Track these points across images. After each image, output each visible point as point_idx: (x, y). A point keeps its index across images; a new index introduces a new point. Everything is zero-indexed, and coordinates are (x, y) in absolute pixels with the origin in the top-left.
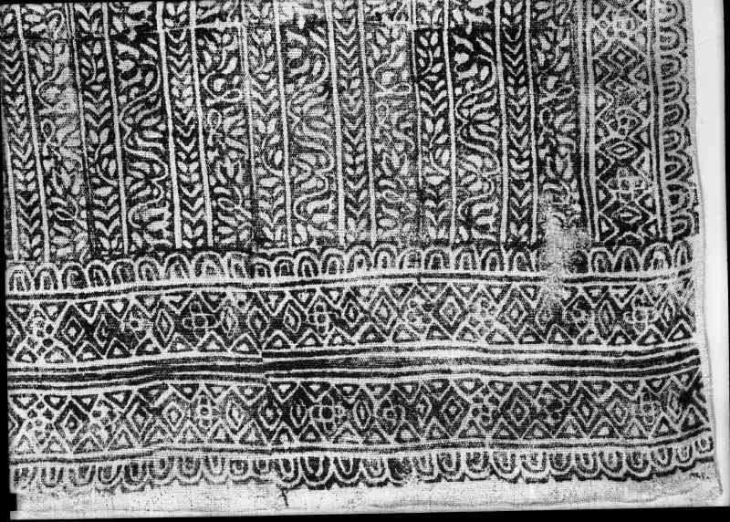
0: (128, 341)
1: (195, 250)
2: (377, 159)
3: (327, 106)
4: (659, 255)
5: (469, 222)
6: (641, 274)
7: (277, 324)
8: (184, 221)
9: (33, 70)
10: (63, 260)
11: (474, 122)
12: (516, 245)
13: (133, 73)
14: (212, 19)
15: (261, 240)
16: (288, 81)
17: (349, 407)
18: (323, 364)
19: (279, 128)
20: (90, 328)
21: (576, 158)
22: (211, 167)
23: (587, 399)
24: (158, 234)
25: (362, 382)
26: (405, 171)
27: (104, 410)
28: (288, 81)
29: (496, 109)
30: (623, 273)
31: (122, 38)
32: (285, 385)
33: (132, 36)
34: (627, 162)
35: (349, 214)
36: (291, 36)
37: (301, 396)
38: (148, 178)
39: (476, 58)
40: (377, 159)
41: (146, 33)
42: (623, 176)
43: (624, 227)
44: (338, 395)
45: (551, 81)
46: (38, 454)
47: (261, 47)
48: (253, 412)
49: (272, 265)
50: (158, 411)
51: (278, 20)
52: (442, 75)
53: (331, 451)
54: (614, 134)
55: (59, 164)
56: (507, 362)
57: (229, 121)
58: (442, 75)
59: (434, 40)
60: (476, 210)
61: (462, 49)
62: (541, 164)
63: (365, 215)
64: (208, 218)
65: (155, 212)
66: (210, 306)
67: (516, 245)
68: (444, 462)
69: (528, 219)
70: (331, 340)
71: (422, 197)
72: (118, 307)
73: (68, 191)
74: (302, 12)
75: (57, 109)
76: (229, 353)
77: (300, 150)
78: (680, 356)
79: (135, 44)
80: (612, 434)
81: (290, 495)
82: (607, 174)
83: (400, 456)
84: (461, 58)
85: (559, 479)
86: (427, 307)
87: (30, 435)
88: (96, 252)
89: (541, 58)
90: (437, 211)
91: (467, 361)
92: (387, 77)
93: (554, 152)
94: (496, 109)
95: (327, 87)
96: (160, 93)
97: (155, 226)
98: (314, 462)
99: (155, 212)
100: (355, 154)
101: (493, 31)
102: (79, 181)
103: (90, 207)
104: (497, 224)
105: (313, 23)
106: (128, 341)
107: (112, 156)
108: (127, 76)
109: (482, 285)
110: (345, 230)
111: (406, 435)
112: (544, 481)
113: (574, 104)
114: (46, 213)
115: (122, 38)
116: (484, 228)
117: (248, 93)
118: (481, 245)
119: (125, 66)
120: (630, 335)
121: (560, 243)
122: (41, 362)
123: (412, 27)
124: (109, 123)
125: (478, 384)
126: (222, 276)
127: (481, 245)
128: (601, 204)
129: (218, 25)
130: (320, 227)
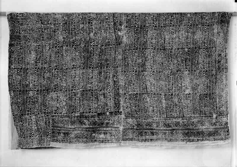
0: (170, 126)
1: (177, 117)
2: (196, 108)
3: (191, 103)
4: (225, 117)
5: (205, 114)
6: (223, 119)
7: (186, 125)
8: (176, 114)
9: (160, 98)
10: (163, 118)
11: (206, 104)
12: (210, 116)
13: (170, 99)
14: (179, 93)
15: (184, 116)
16: (187, 100)
17: (193, 134)
18: (190, 129)
19: (186, 105)
20: (166, 125)
21: (216, 107)
22: (179, 109)
23: (217, 132)
24: (173, 116)
25: (194, 131)
26: (199, 109)
27: (168, 134)
28: (187, 100)
29: (208, 102)
30: (221, 119)
31: (170, 95)
32: (186, 131)
33: (171, 95)
34: (222, 107)
35: (193, 114)
36: (187, 95)
37: (188, 133)
38: (172, 110)
39: (206, 97)
40: (196, 108)
41: (172, 95)
42: (221, 108)
43: (221, 114)
44: (192, 132)
45: (214, 99)
46: (161, 138)
47: (184, 96)
48: (183, 134)
49: (185, 119)
50: (173, 134)
51: (186, 93)
52: (203, 99)
53: (191, 138)
54: (220, 104)
55: (163, 108)
56: (209, 129)
57: (180, 104)
58: (203, 99)
59: (202, 95)
60: (206, 113)
61: (205, 96)
62: (213, 108)
63: (195, 114)
64: (178, 114)
65: (173, 113)
66: (179, 123)
67: (210, 116)
68: (203, 139)
69: (211, 114)
70: (191, 127)
71: (200, 112)
72: (169, 123)
73: (164, 111)
74: (188, 93)
75: (163, 102)
76: (180, 128)
77: (188, 107)
78: (227, 127)
79: (171, 96)
80: (220, 135)
81: (187, 143)
82: (219, 108)
83: (198, 139)
84: (205, 97)
85: (214, 140)
86: (201, 123)
87: (160, 135)
88: (167, 117)
89: (213, 97)
90: (202, 113)
91: (205, 129)
92: (197, 99)
93: (214, 107)
94: (208, 102)
95: (191, 100)
96: (173, 101)
97: (173, 115)
98: (189, 139)
99: (173, 113)
100: (158, 40)
101: (208, 94)
102: (165, 110)
103: (166, 112)
104: (208, 114)
105: (189, 94)
106: (170, 126)
107: (168, 107)
108: (170, 99)
109: (207, 121)
110: (193, 115)
111: (199, 136)
112: (213, 141)
113: (216, 101)
114: (162, 113)
115: (170, 95)
116: (207, 115)
117: (182, 101)
118: (206, 116)
119: (170, 98)
120: (222, 125)
121: (215, 116)
122: (161, 128)
123: (199, 94)
124: (168, 104)
125: (206, 131)
126: (180, 120)
127: (206, 116)
128: (219, 112)
129: (179, 94)
130: (190, 115)
